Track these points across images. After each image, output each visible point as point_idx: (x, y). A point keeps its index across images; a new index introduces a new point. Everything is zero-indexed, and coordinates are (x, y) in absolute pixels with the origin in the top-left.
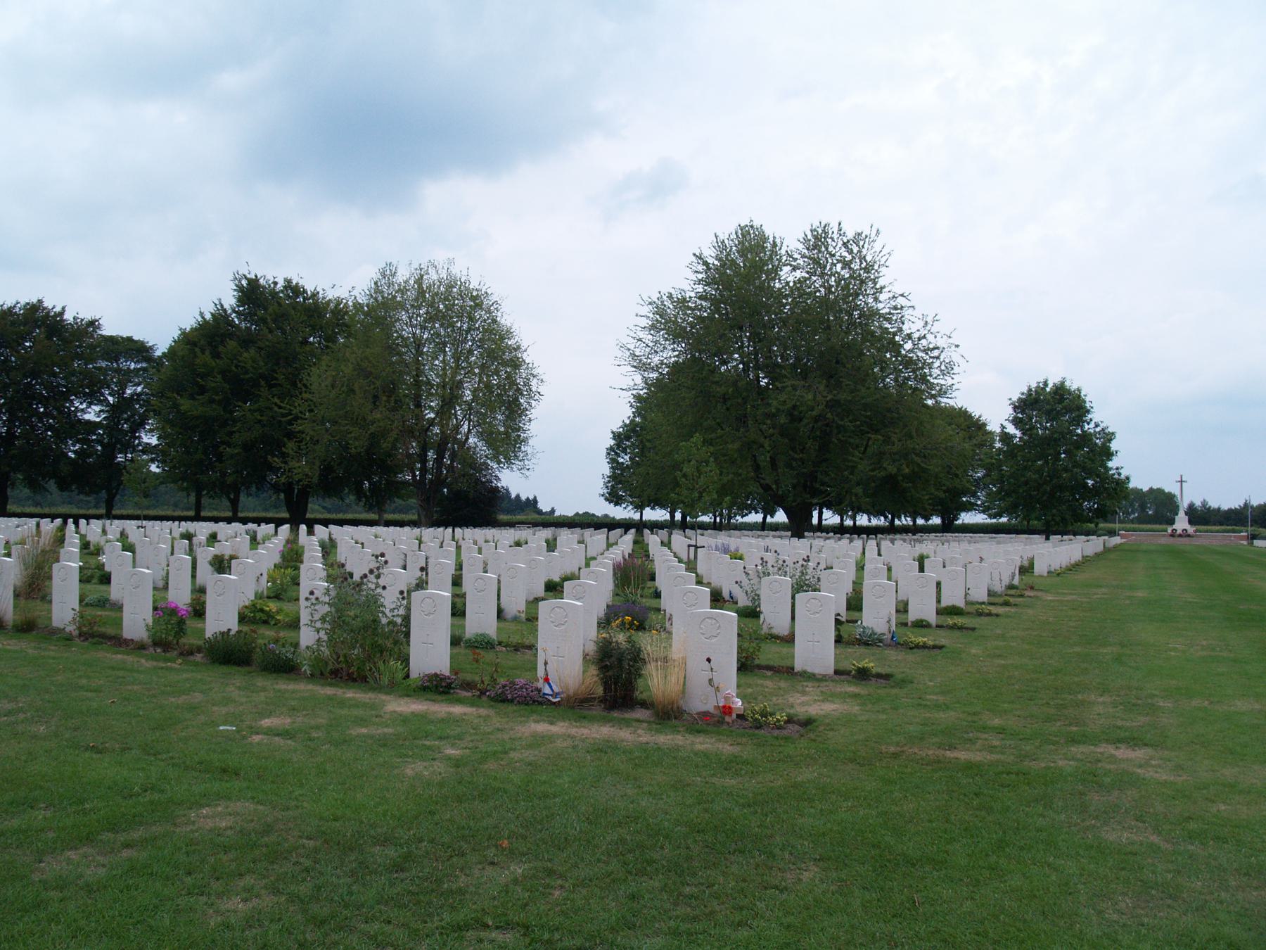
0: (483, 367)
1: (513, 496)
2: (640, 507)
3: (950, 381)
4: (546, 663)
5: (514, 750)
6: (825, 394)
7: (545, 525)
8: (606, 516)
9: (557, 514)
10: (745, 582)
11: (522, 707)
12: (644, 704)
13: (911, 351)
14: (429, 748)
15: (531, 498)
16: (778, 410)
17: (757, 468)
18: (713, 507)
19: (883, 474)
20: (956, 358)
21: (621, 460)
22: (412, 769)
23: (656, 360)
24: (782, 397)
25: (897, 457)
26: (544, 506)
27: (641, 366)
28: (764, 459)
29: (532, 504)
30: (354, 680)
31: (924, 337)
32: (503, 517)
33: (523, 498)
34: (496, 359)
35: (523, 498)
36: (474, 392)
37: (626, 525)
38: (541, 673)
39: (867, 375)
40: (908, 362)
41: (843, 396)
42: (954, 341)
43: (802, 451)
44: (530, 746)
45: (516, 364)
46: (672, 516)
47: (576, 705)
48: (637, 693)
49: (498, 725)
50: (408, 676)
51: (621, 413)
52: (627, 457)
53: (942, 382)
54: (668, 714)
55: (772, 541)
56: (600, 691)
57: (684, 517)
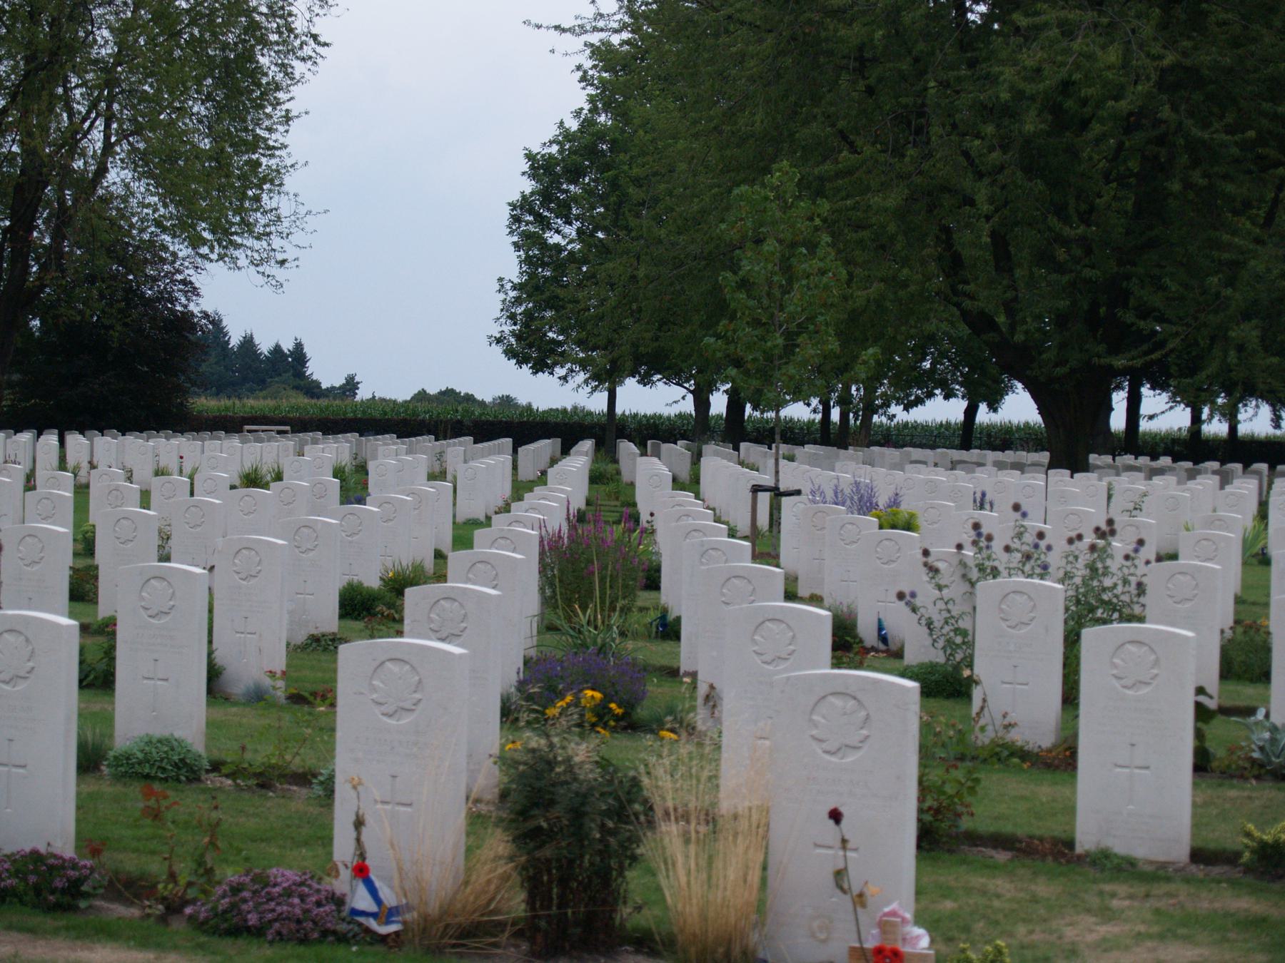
1: (235, 340)
2: (608, 377)
4: (359, 824)
6: (1156, 49)
7: (331, 426)
9: (363, 394)
15: (287, 346)
16: (1019, 95)
17: (954, 264)
21: (554, 239)
24: (1031, 57)
26: (325, 371)
28: (974, 241)
29: (290, 364)
32: (204, 403)
33: (264, 346)
36: (123, 32)
37: (566, 429)
38: (343, 850)
43: (1085, 218)
46: (702, 403)
48: (626, 911)
51: (556, 99)
52: (571, 231)
56: (516, 904)
57: (735, 406)
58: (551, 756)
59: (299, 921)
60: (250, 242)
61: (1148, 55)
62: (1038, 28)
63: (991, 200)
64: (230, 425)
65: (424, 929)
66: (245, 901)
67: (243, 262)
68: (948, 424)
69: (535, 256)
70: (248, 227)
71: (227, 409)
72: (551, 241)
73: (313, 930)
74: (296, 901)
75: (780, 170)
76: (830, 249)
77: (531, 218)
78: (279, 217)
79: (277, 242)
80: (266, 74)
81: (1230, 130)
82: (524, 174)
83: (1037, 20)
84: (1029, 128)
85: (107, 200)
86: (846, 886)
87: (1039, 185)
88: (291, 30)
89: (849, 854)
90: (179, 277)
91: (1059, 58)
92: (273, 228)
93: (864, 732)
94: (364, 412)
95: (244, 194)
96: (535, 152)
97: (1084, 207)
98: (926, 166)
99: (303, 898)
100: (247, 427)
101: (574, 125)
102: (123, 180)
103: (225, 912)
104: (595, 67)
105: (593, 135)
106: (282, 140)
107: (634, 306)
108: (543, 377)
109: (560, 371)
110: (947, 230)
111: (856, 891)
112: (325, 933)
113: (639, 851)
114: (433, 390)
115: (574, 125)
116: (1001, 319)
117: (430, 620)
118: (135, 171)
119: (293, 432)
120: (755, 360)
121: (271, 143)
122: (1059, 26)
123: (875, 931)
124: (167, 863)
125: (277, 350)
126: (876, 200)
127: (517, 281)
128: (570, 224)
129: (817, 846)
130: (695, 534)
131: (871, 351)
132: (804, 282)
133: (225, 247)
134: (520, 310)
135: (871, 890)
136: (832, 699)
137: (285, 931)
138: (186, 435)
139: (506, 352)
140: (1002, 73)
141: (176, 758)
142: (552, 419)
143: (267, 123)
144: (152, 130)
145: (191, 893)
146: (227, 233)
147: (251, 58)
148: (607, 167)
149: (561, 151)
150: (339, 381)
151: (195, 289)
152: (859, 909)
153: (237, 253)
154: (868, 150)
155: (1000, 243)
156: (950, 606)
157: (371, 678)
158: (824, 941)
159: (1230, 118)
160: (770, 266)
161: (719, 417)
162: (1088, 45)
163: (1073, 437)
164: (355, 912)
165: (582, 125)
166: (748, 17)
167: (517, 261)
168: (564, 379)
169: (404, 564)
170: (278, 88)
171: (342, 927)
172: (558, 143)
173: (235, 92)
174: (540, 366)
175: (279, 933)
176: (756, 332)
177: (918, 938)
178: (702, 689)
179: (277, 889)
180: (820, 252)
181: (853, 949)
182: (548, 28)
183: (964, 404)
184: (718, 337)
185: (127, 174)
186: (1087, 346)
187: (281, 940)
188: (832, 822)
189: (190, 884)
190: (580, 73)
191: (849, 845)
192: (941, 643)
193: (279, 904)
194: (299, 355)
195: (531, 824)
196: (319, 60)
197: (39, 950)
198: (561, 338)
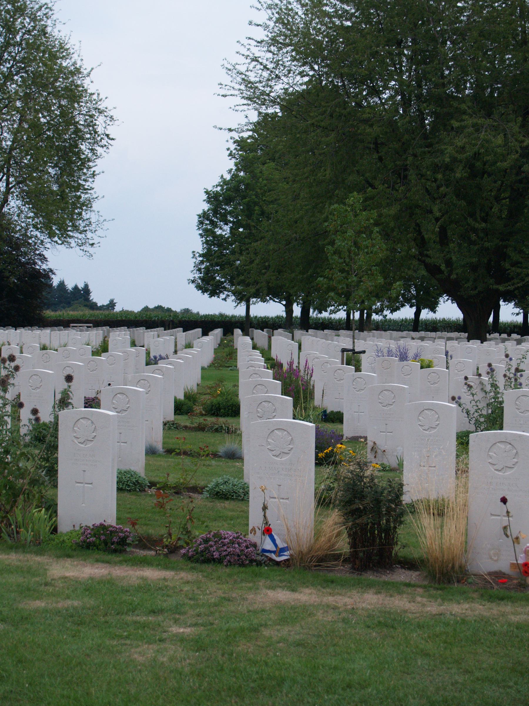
0: (27, 98)
1: (55, 282)
2: (242, 297)
4: (265, 508)
5: (266, 626)
6: (521, 138)
7: (97, 324)
8: (187, 311)
9: (118, 309)
10: (466, 398)
12: (410, 564)
14: (144, 626)
15: (81, 286)
16: (454, 160)
18: (346, 298)
21: (219, 232)
22: (142, 653)
23: (278, 88)
24: (460, 142)
26: (99, 298)
27: (255, 95)
28: (431, 230)
29: (82, 295)
32: (49, 313)
33: (70, 286)
34: (45, 87)
35: (70, 286)
36: (15, 133)
37: (207, 324)
38: (255, 519)
43: (484, 220)
44: (283, 621)
45: (74, 94)
46: (289, 310)
47: (311, 564)
48: (396, 548)
49: (220, 593)
50: (55, 530)
51: (218, 166)
52: (227, 228)
54: (446, 575)
55: (433, 347)
56: (343, 545)
57: (305, 312)
58: (362, 474)
59: (239, 556)
60: (76, 235)
61: (516, 140)
63: (440, 210)
64: (65, 324)
66: (211, 546)
67: (73, 244)
68: (406, 319)
69: (210, 240)
70: (76, 228)
71: (60, 316)
73: (246, 560)
74: (237, 546)
75: (353, 197)
76: (378, 234)
77: (208, 222)
78: (90, 222)
79: (89, 235)
82: (204, 200)
83: (463, 123)
84: (458, 175)
86: (509, 533)
88: (96, 132)
89: (510, 519)
90: (37, 252)
91: (473, 142)
92: (87, 228)
93: (515, 460)
94: (126, 317)
96: (209, 190)
97: (483, 214)
98: (408, 195)
99: (239, 544)
100: (72, 325)
101: (228, 177)
102: (17, 206)
103: (202, 551)
104: (235, 149)
105: (237, 181)
106: (91, 185)
107: (267, 264)
109: (222, 296)
110: (418, 225)
111: (514, 536)
112: (252, 561)
113: (402, 519)
114: (151, 306)
115: (228, 177)
116: (443, 267)
117: (258, 412)
119: (94, 327)
120: (343, 288)
121: (86, 187)
123: (523, 555)
124: (168, 528)
125: (76, 288)
126: (385, 211)
127: (201, 252)
128: (227, 225)
129: (492, 515)
130: (255, 375)
131: (398, 283)
132: (366, 250)
133: (65, 238)
134: (203, 267)
135: (522, 536)
136: (498, 444)
137: (232, 560)
138: (26, 328)
139: (196, 287)
140: (446, 149)
142: (216, 319)
143: (83, 177)
144: (31, 181)
145: (180, 543)
147: (76, 146)
148: (244, 197)
149: (222, 190)
150: (106, 302)
151: (45, 258)
152: (516, 544)
153: (71, 241)
154: (381, 187)
155: (443, 231)
156: (478, 404)
157: (268, 438)
160: (350, 243)
161: (296, 317)
162: (487, 136)
163: (477, 325)
164: (264, 551)
165: (232, 177)
166: (322, 124)
167: (201, 243)
168: (225, 299)
169: (189, 388)
170: (89, 160)
171: (259, 558)
172: (221, 186)
173: (70, 162)
174: (213, 293)
175: (229, 561)
176: (343, 275)
178: (370, 444)
179: (226, 540)
180: (373, 236)
181: (512, 564)
182: (225, 129)
183: (414, 309)
184: (325, 277)
185: (19, 203)
186: (486, 281)
187: (231, 565)
188: (502, 503)
189: (179, 539)
190: (229, 152)
191: (510, 515)
192: (473, 422)
193: (228, 547)
194: (87, 290)
195: (354, 507)
196: (110, 147)
197: (118, 571)
198: (223, 280)
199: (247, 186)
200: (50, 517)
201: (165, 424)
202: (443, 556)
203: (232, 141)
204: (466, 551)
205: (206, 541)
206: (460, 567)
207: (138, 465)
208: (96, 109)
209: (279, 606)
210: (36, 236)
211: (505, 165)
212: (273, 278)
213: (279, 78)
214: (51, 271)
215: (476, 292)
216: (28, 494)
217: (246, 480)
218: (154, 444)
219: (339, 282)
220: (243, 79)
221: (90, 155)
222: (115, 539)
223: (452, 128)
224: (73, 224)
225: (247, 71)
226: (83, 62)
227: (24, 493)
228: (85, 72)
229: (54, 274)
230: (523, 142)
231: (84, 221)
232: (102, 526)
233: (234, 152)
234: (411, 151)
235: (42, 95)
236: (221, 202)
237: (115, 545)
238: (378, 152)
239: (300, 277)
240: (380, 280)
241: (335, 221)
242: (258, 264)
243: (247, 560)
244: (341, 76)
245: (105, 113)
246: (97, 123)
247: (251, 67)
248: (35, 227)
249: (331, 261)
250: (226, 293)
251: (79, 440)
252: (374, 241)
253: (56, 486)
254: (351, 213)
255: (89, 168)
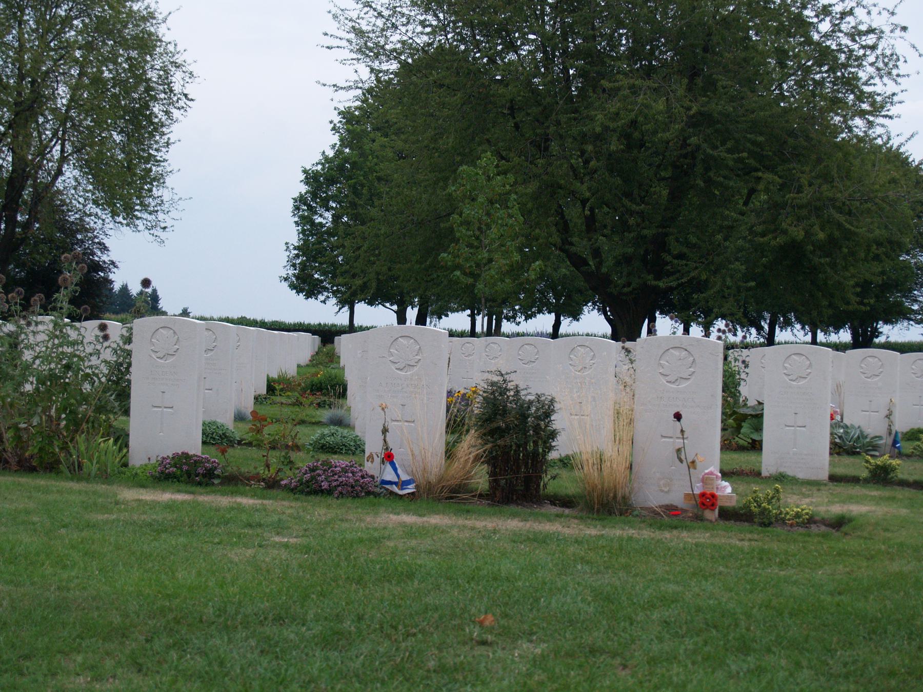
1: (117, 287)
2: (348, 301)
3: (891, 87)
4: (385, 431)
6: (687, 103)
11: (349, 502)
13: (826, 36)
16: (606, 128)
17: (564, 227)
19: (781, 240)
20: (901, 48)
21: (319, 220)
23: (394, 40)
24: (614, 106)
25: (804, 212)
27: (368, 48)
30: (32, 470)
31: (851, 13)
34: (110, 34)
39: (757, 73)
40: (824, 55)
41: (717, 107)
42: (898, 20)
45: (147, 44)
47: (449, 494)
51: (320, 142)
52: (328, 215)
53: (879, 89)
54: (606, 503)
56: (481, 478)
59: (352, 487)
60: (146, 216)
62: (619, 89)
65: (429, 490)
66: (320, 475)
67: (141, 227)
70: (145, 207)
72: (317, 221)
74: (350, 475)
78: (162, 201)
79: (161, 216)
80: (156, 117)
81: (729, 151)
83: (616, 84)
84: (613, 147)
85: (59, 192)
86: (683, 457)
87: (619, 181)
88: (171, 91)
90: (97, 240)
95: (143, 188)
98: (550, 170)
99: (353, 472)
101: (331, 153)
102: (74, 176)
103: (307, 481)
104: (340, 122)
107: (377, 252)
108: (312, 301)
109: (321, 298)
111: (690, 460)
113: (553, 444)
115: (331, 153)
118: (81, 171)
120: (471, 266)
121: (158, 158)
122: (629, 88)
127: (296, 244)
131: (537, 263)
139: (290, 286)
141: (221, 432)
143: (155, 146)
146: (133, 210)
152: (691, 470)
153: (137, 222)
154: (516, 160)
158: (668, 492)
159: (729, 144)
164: (384, 482)
166: (447, 82)
170: (162, 126)
171: (378, 490)
172: (323, 164)
173: (139, 127)
175: (341, 493)
177: (725, 487)
181: (687, 495)
183: (552, 317)
185: (76, 173)
190: (332, 125)
193: (340, 477)
195: (494, 425)
196: (188, 109)
199: (354, 165)
200: (120, 450)
201: (256, 398)
202: (603, 483)
203: (336, 112)
204: (630, 480)
205: (313, 470)
206: (624, 497)
207: (226, 420)
208: (172, 63)
209: (403, 525)
210: (97, 214)
211: (667, 135)
212: (385, 269)
213: (397, 28)
214: (113, 263)
215: (630, 289)
216: (93, 422)
217: (358, 432)
218: (243, 410)
219: (467, 260)
220: (353, 27)
221: (164, 118)
222: (200, 471)
223: (604, 91)
224: (141, 202)
225: (358, 18)
226: (159, 5)
227: (87, 422)
228: (160, 17)
229: (116, 267)
230: (689, 109)
231: (155, 198)
232: (186, 455)
233: (338, 125)
234: (553, 117)
235: (107, 44)
236: (322, 184)
237: (201, 477)
238: (514, 118)
239: (417, 267)
240: (517, 257)
241: (464, 185)
242: (366, 252)
243: (364, 491)
244: (472, 27)
245: (184, 69)
246: (174, 79)
247: (362, 15)
248: (96, 202)
249: (458, 235)
250: (326, 294)
251: (159, 355)
252: (510, 211)
253: (127, 412)
254: (483, 177)
255: (163, 134)
